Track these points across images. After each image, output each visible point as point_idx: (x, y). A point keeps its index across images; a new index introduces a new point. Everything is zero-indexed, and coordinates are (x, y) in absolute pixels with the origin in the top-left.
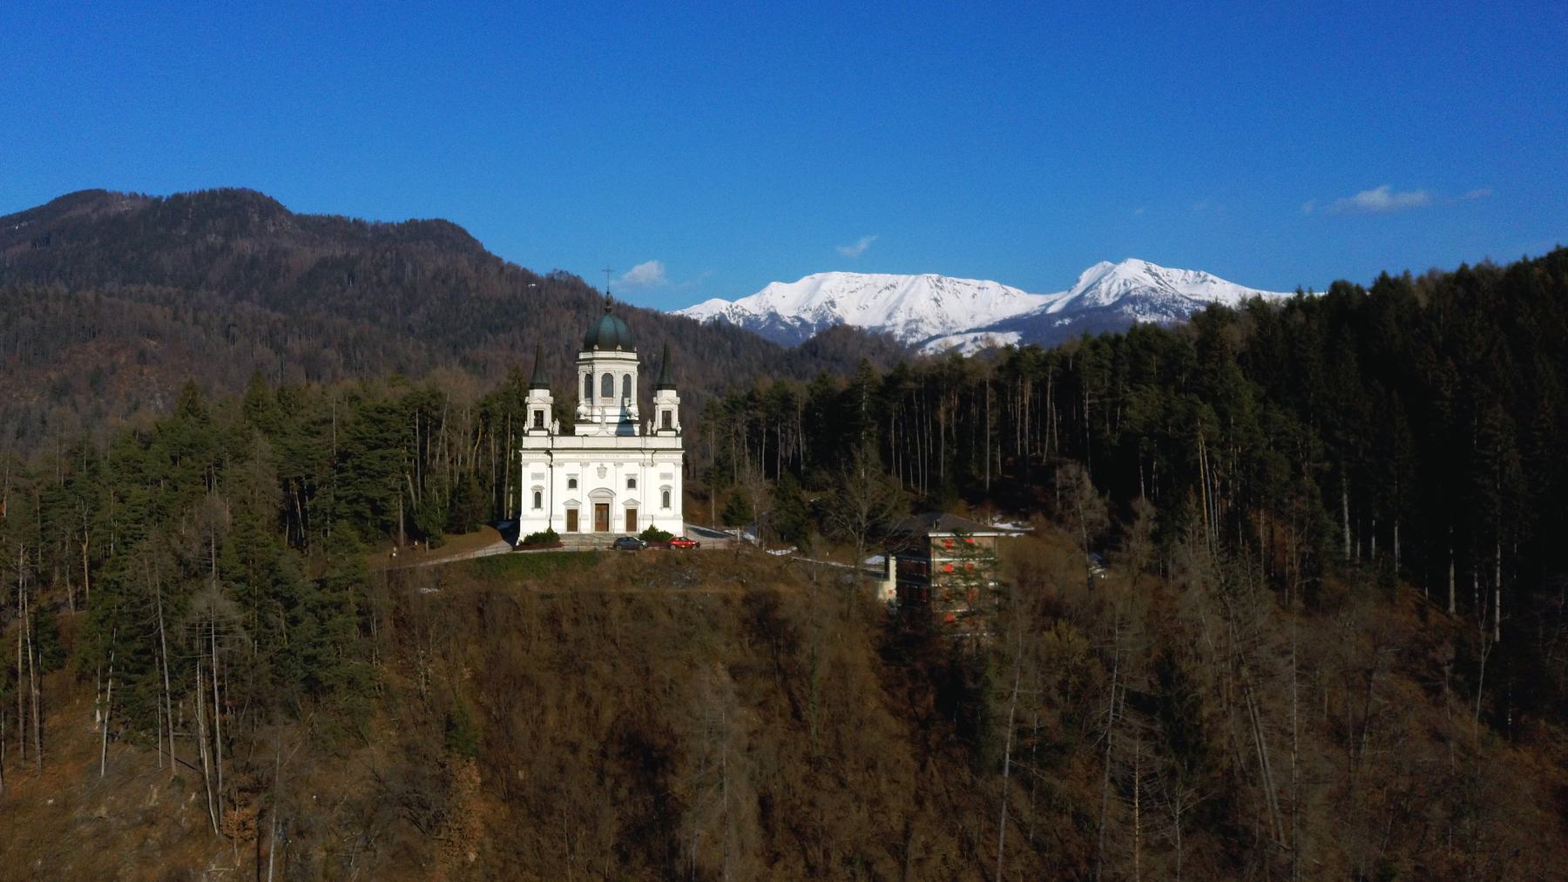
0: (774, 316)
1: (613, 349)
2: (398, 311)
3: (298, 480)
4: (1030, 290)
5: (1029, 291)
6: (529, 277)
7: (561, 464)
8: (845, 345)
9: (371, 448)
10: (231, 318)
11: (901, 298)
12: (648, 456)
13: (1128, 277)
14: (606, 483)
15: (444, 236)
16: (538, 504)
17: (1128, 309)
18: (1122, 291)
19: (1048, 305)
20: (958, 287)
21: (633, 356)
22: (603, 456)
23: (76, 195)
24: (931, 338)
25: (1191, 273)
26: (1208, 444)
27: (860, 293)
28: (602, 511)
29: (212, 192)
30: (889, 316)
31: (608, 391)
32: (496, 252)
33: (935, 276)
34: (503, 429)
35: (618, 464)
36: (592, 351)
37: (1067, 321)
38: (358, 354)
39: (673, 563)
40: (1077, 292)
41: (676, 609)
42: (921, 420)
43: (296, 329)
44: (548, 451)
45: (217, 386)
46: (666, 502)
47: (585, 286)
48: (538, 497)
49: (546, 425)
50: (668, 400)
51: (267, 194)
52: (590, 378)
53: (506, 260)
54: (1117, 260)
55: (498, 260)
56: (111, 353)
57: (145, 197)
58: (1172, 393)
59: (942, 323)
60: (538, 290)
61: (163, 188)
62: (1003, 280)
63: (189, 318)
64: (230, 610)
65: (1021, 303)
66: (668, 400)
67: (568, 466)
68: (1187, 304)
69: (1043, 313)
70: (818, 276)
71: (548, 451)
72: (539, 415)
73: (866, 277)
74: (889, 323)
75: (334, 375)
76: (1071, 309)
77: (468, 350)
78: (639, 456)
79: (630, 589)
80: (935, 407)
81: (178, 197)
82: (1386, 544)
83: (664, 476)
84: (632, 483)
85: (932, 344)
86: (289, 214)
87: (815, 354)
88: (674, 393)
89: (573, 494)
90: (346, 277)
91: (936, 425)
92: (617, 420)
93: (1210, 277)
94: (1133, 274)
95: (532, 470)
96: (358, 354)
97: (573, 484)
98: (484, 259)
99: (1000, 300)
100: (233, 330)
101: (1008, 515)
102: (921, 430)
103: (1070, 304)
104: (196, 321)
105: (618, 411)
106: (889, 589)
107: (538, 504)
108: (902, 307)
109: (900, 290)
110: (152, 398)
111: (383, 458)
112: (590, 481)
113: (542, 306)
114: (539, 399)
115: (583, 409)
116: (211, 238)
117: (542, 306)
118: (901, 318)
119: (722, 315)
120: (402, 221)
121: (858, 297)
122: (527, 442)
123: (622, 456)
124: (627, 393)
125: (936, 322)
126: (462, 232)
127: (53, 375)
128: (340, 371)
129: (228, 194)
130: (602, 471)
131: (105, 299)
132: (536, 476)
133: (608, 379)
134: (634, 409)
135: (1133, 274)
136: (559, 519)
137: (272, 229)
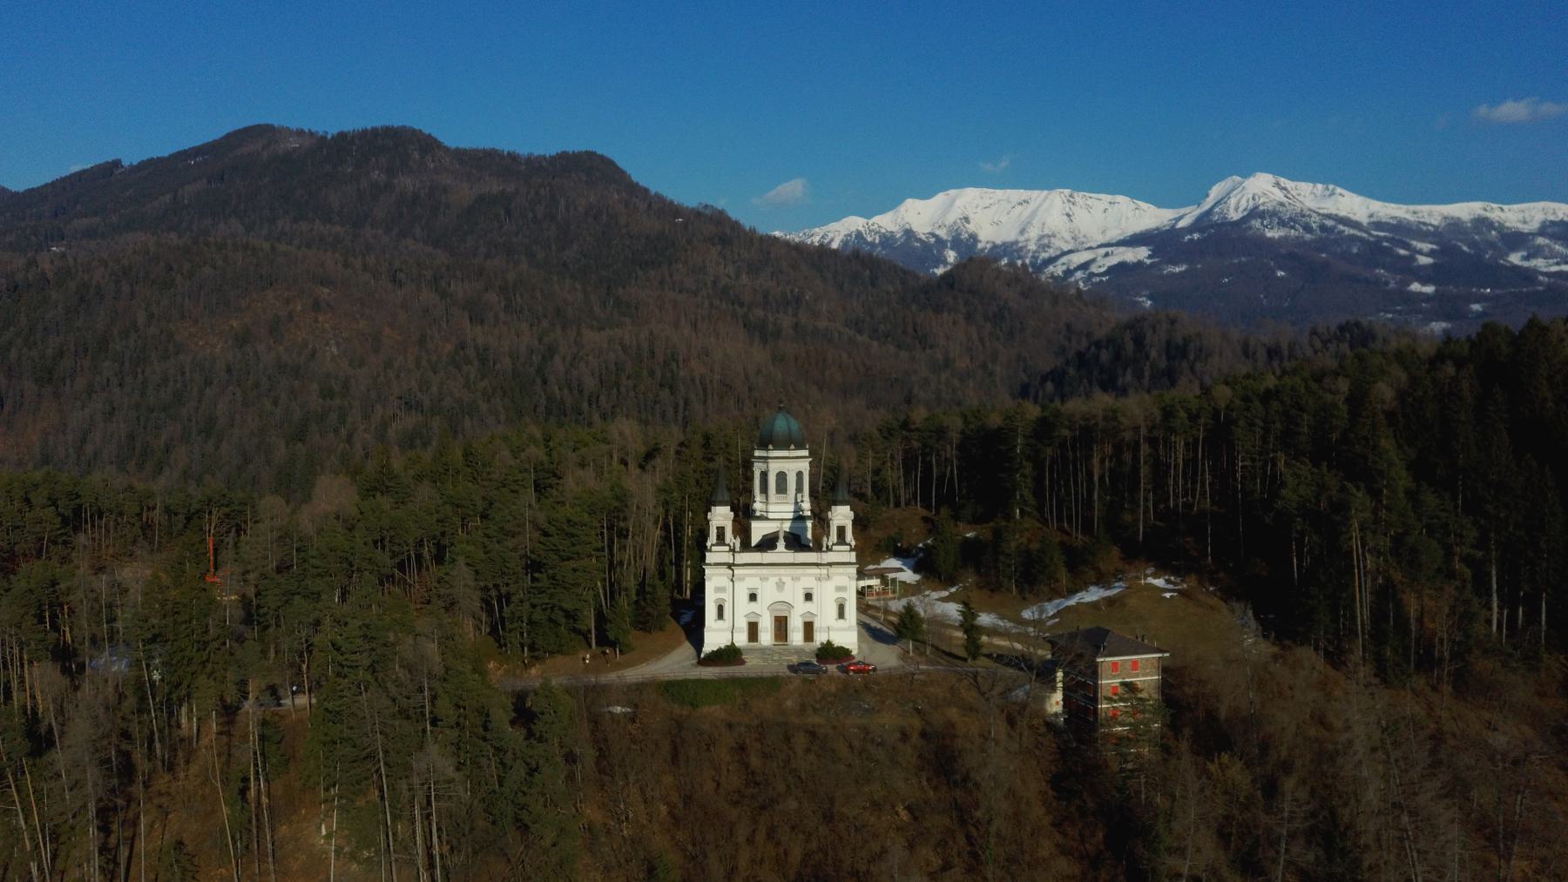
0: (909, 233)
1: (788, 449)
3: (496, 586)
4: (1160, 204)
5: (1159, 205)
8: (981, 277)
9: (563, 559)
11: (1034, 214)
12: (824, 571)
14: (785, 596)
15: (593, 169)
16: (720, 615)
18: (1251, 203)
20: (1089, 202)
21: (805, 453)
22: (782, 570)
23: (247, 130)
24: (1064, 254)
25: (1320, 186)
26: (1362, 529)
28: (781, 625)
29: (374, 130)
30: (1022, 232)
31: (782, 488)
32: (643, 183)
33: (1067, 192)
34: (684, 552)
35: (796, 579)
37: (1196, 236)
40: (1206, 206)
41: (856, 743)
42: (1075, 469)
43: (458, 273)
44: (730, 566)
45: (387, 330)
46: (841, 615)
51: (426, 131)
52: (764, 475)
53: (653, 191)
54: (1246, 174)
55: (646, 190)
56: (288, 301)
57: (311, 134)
58: (1325, 469)
60: (685, 225)
62: (1135, 194)
63: (358, 263)
64: (447, 767)
65: (1151, 217)
66: (842, 515)
67: (749, 580)
69: (1173, 226)
70: (952, 192)
71: (730, 566)
72: (721, 532)
73: (999, 193)
74: (1021, 239)
76: (1200, 224)
78: (815, 571)
79: (814, 719)
80: (1089, 458)
81: (342, 135)
82: (1533, 616)
83: (839, 589)
84: (808, 597)
85: (1064, 259)
86: (447, 149)
87: (951, 286)
89: (753, 606)
91: (1090, 475)
92: (791, 516)
93: (1339, 190)
94: (1262, 188)
95: (716, 584)
97: (753, 597)
98: (634, 189)
100: (401, 276)
101: (1162, 568)
102: (1076, 475)
104: (365, 268)
105: (792, 508)
106: (1055, 702)
107: (720, 615)
110: (327, 344)
111: (575, 570)
113: (689, 242)
114: (721, 516)
115: (758, 506)
116: (375, 175)
117: (689, 242)
118: (1033, 233)
120: (553, 153)
121: (989, 213)
122: (710, 558)
124: (799, 489)
125: (1067, 236)
128: (502, 315)
129: (389, 132)
130: (780, 586)
132: (719, 590)
133: (782, 477)
135: (1262, 188)
136: (740, 630)
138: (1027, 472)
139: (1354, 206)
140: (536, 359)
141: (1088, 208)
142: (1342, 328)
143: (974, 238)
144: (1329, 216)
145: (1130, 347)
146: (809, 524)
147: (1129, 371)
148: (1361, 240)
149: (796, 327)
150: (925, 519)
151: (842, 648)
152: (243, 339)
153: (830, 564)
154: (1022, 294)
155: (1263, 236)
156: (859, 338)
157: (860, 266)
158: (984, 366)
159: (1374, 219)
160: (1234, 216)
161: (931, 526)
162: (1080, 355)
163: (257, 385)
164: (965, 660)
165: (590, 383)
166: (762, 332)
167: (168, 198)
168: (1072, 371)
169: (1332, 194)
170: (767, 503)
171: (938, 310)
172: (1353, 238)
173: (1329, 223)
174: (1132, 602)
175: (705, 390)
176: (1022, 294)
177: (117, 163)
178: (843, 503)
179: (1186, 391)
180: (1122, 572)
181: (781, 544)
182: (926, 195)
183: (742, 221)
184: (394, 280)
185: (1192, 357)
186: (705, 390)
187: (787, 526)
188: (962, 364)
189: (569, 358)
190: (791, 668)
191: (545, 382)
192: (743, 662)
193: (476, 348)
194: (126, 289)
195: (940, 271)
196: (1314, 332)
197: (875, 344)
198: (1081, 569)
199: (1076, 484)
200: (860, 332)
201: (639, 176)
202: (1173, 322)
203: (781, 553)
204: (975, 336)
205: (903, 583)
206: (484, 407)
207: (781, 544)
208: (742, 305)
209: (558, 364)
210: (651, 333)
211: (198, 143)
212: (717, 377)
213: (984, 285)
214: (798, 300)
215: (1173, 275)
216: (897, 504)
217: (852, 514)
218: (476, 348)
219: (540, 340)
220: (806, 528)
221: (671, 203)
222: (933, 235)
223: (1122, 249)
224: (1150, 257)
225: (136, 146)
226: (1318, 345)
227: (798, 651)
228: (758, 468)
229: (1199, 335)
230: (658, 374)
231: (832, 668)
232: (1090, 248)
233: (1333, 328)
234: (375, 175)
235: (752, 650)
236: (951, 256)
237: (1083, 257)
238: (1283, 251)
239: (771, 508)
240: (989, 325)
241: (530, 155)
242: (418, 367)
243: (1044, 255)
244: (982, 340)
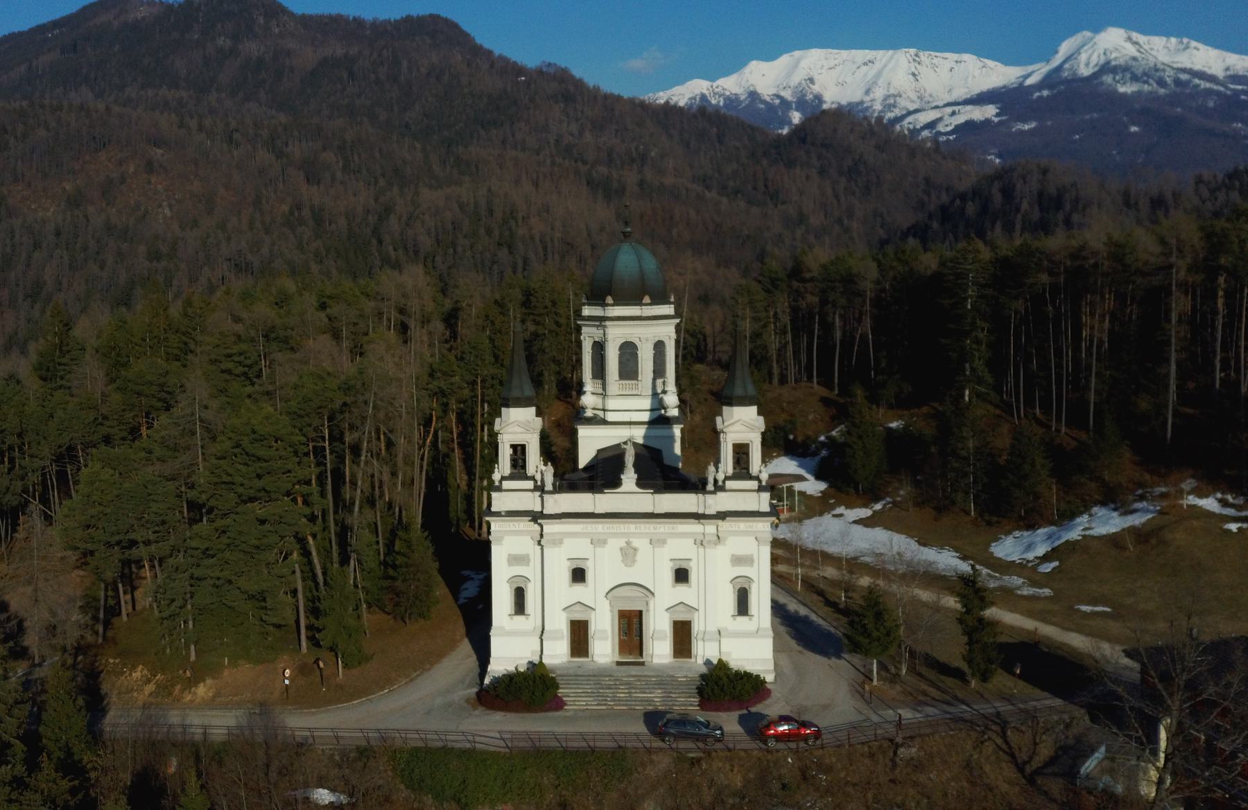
0: (753, 95)
1: (638, 302)
2: (396, 108)
5: (1007, 62)
6: (519, 70)
7: (558, 542)
8: (835, 130)
10: (233, 124)
11: (879, 74)
12: (710, 528)
13: (1107, 46)
17: (1108, 79)
18: (1102, 60)
19: (1029, 75)
20: (935, 61)
21: (668, 309)
22: (631, 526)
24: (910, 113)
25: (1173, 40)
27: (839, 69)
28: (631, 627)
30: (867, 92)
31: (629, 370)
32: (487, 45)
33: (913, 51)
36: (604, 305)
37: (1045, 93)
38: (356, 158)
39: (775, 786)
40: (1056, 62)
43: (296, 133)
44: (536, 517)
46: (743, 606)
47: (572, 77)
48: (520, 596)
49: (531, 470)
50: (742, 424)
52: (599, 348)
53: (497, 52)
54: (1097, 29)
55: (490, 53)
56: (120, 163)
59: (920, 98)
62: (982, 53)
63: (193, 124)
65: (999, 75)
66: (742, 424)
67: (571, 542)
68: (1169, 72)
69: (1021, 84)
70: (797, 53)
71: (536, 517)
72: (519, 451)
74: (867, 99)
75: (333, 178)
76: (1049, 81)
77: (461, 149)
83: (738, 560)
84: (681, 576)
85: (910, 119)
86: (291, 14)
87: (803, 141)
88: (753, 410)
90: (345, 76)
92: (645, 417)
93: (1194, 44)
95: (509, 549)
96: (356, 158)
97: (579, 575)
98: (477, 52)
99: (977, 73)
100: (236, 136)
101: (1211, 482)
103: (1048, 76)
104: (201, 128)
105: (647, 403)
108: (880, 82)
109: (878, 65)
112: (607, 570)
114: (519, 425)
115: (589, 400)
116: (221, 41)
118: (879, 93)
119: (703, 97)
120: (398, 17)
121: (834, 75)
122: (500, 502)
123: (663, 527)
124: (659, 371)
125: (914, 96)
126: (454, 26)
127: (68, 187)
128: (339, 175)
130: (629, 554)
131: (116, 109)
132: (515, 560)
133: (629, 351)
134: (671, 399)
136: (556, 636)
137: (277, 30)
138: (982, 335)
139: (1209, 60)
140: (372, 219)
141: (934, 66)
142: (1230, 176)
143: (819, 98)
144: (1184, 70)
145: (998, 198)
146: (677, 430)
147: (999, 224)
148: (1218, 93)
149: (641, 183)
150: (825, 401)
151: (747, 675)
152: (75, 201)
153: (722, 516)
154: (878, 147)
155: (1116, 91)
156: (708, 194)
157: (707, 122)
158: (840, 221)
159: (1231, 73)
160: (1085, 72)
161: (839, 411)
162: (944, 209)
164: (957, 674)
165: (426, 242)
166: (605, 189)
168: (935, 225)
169: (1187, 47)
170: (604, 395)
171: (790, 164)
172: (1209, 92)
173: (1184, 77)
174: (1179, 537)
175: (545, 248)
176: (878, 147)
178: (744, 401)
179: (1056, 242)
180: (1141, 485)
181: (629, 478)
182: (770, 56)
183: (586, 80)
184: (230, 140)
185: (1068, 207)
186: (545, 248)
187: (639, 434)
188: (816, 220)
189: (405, 218)
190: (653, 719)
191: (380, 242)
192: (559, 704)
193: (312, 208)
195: (785, 131)
196: (1199, 181)
197: (725, 200)
198: (1081, 485)
199: (1059, 353)
200: (708, 188)
201: (484, 39)
202: (1045, 172)
203: (629, 494)
204: (829, 192)
205: (802, 494)
206: (314, 267)
207: (629, 478)
208: (585, 163)
209: (394, 223)
210: (489, 190)
211: (57, 15)
212: (558, 235)
213: (836, 141)
214: (643, 157)
215: (1022, 132)
216: (783, 380)
217: (760, 423)
218: (312, 208)
219: (376, 200)
220: (671, 438)
221: (515, 63)
222: (778, 96)
223: (969, 108)
224: (997, 115)
226: (1206, 193)
227: (664, 680)
228: (589, 336)
229: (1074, 185)
230: (496, 233)
231: (729, 722)
232: (937, 107)
233: (1220, 177)
234: (221, 41)
235: (576, 677)
236: (796, 117)
237: (930, 116)
238: (1137, 106)
239: (612, 404)
240: (843, 180)
241: (375, 20)
242: (251, 228)
243: (890, 115)
244: (836, 196)
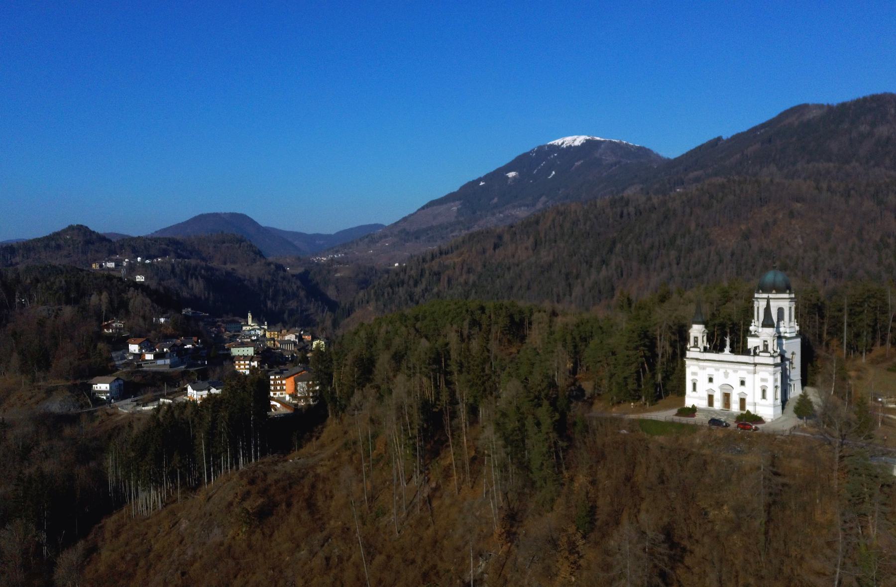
16: (694, 389)
28: (727, 397)
35: (704, 368)
46: (764, 397)
56: (775, 212)
61: (835, 99)
63: (824, 186)
67: (711, 369)
72: (696, 339)
81: (843, 105)
83: (763, 380)
84: (742, 383)
89: (710, 386)
97: (711, 380)
104: (829, 189)
107: (694, 389)
112: (719, 380)
122: (689, 354)
123: (737, 366)
127: (743, 227)
130: (726, 375)
152: (746, 236)
163: (746, 263)
167: (738, 156)
177: (719, 139)
194: (688, 210)
225: (729, 127)
